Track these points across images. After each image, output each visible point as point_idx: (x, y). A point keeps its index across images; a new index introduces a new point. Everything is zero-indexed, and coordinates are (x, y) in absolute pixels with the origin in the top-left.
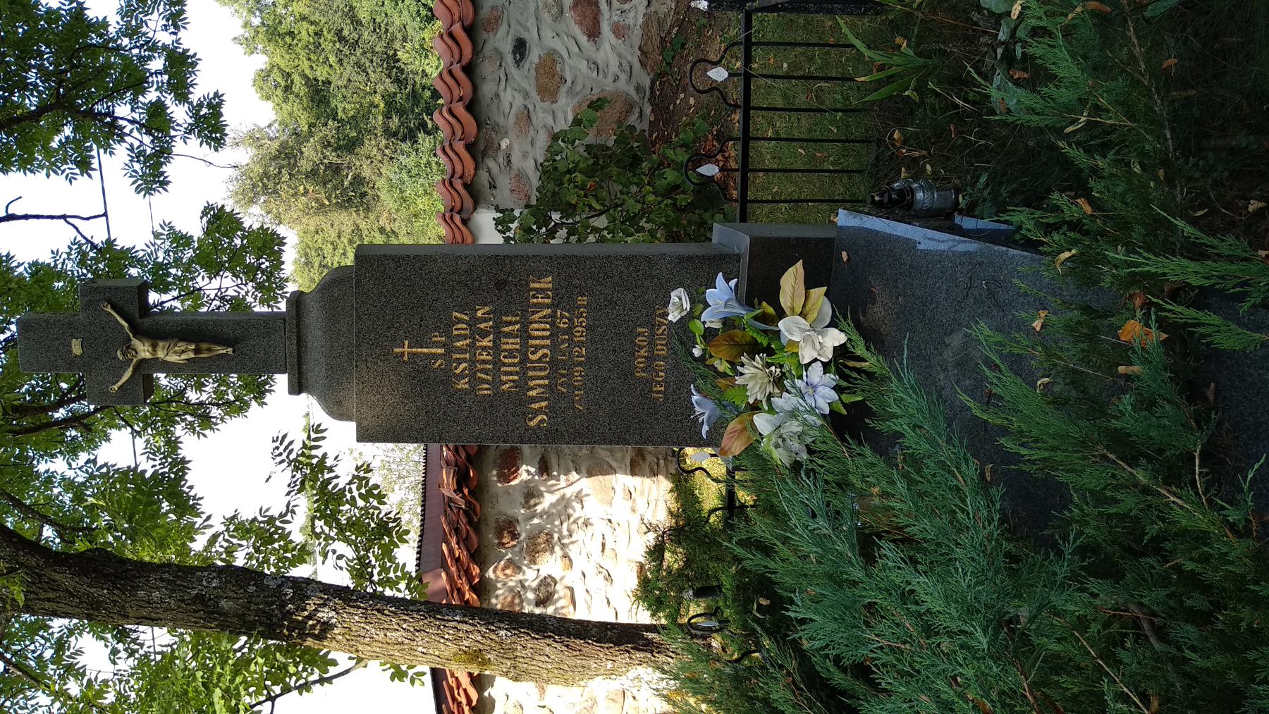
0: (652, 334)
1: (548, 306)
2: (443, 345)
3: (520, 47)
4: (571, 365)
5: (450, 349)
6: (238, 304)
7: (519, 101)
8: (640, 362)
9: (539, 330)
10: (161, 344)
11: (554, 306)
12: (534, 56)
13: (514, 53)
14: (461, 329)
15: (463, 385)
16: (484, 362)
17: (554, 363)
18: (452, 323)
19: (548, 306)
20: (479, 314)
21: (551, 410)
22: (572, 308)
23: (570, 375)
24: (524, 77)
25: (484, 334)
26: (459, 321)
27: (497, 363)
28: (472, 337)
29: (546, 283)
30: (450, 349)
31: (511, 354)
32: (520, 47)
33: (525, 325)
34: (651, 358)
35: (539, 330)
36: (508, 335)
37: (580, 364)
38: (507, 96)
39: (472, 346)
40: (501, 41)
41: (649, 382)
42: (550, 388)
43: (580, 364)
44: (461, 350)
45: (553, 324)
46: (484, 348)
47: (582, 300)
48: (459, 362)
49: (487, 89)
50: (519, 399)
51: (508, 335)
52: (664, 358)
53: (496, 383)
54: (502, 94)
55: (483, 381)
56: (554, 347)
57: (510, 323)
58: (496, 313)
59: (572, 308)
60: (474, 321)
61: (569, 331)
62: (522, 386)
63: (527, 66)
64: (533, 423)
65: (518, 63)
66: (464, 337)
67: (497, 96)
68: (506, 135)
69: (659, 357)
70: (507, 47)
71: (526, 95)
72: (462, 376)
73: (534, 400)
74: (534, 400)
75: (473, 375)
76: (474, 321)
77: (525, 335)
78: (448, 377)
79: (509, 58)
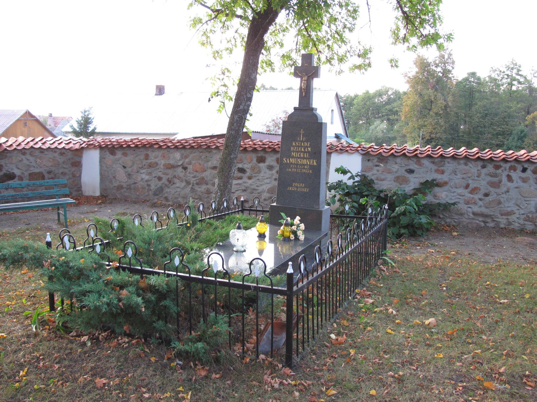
0: (303, 187)
1: (310, 164)
2: (302, 140)
3: (411, 171)
4: (297, 168)
5: (301, 142)
6: (138, 305)
7: (395, 170)
8: (296, 184)
9: (305, 162)
10: (306, 82)
11: (310, 165)
12: (408, 175)
13: (410, 169)
14: (306, 144)
15: (294, 144)
16: (298, 149)
17: (297, 165)
18: (307, 142)
19: (310, 164)
20: (309, 148)
21: (287, 164)
22: (310, 169)
23: (294, 168)
24: (402, 172)
25: (304, 149)
26: (307, 144)
27: (298, 152)
28: (304, 146)
29: (315, 164)
30: (301, 142)
31: (300, 155)
32: (411, 171)
33: (306, 158)
34: (297, 187)
35: (305, 162)
36: (304, 155)
37: (297, 170)
38: (396, 167)
39: (302, 146)
40: (413, 166)
41: (292, 186)
42: (292, 163)
43: (297, 170)
44: (301, 144)
45: (306, 165)
46: (301, 149)
47: (311, 171)
48: (299, 143)
49: (398, 160)
50: (290, 156)
51: (304, 155)
52: (297, 190)
53: (294, 151)
54: (397, 165)
55: (294, 149)
56: (301, 165)
57: (306, 155)
58: (309, 152)
59: (310, 169)
60: (307, 147)
61: (304, 168)
62: (293, 157)
63: (406, 173)
64: (284, 159)
65: (406, 171)
66: (304, 145)
67: (396, 163)
68: (385, 166)
69: (297, 189)
70: (412, 167)
71: (396, 172)
72: (295, 144)
73: (289, 160)
74: (289, 160)
75: (295, 146)
76: (307, 147)
77: (304, 158)
78: (296, 141)
79: (408, 168)
